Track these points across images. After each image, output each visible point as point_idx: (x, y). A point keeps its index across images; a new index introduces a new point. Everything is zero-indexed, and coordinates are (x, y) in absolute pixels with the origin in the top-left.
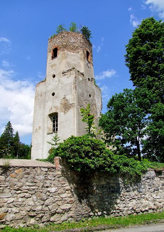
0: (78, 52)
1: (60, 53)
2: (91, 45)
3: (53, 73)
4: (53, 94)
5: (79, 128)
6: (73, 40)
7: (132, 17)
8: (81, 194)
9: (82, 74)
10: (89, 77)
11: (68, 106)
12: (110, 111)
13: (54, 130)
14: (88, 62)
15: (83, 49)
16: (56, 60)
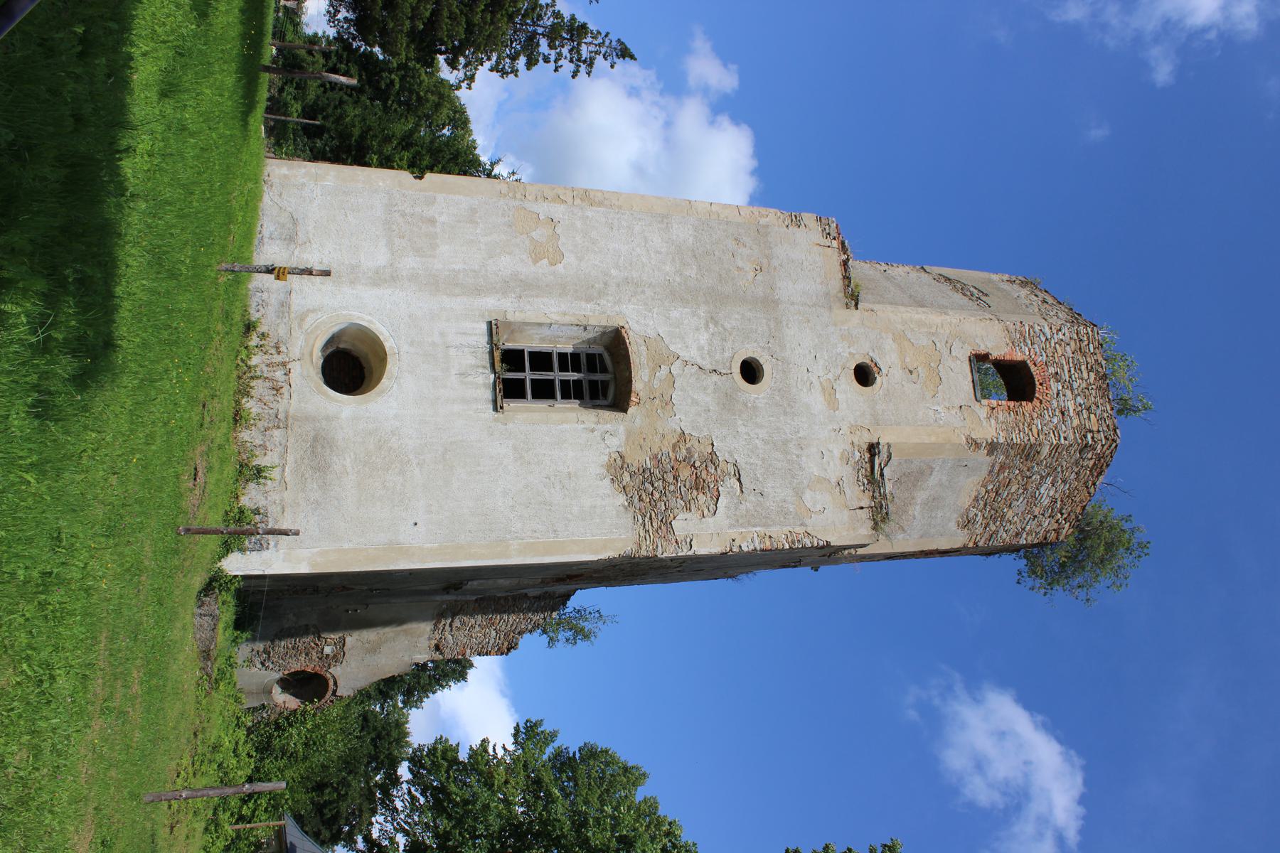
0: (968, 523)
3: (884, 371)
13: (512, 359)
16: (961, 378)
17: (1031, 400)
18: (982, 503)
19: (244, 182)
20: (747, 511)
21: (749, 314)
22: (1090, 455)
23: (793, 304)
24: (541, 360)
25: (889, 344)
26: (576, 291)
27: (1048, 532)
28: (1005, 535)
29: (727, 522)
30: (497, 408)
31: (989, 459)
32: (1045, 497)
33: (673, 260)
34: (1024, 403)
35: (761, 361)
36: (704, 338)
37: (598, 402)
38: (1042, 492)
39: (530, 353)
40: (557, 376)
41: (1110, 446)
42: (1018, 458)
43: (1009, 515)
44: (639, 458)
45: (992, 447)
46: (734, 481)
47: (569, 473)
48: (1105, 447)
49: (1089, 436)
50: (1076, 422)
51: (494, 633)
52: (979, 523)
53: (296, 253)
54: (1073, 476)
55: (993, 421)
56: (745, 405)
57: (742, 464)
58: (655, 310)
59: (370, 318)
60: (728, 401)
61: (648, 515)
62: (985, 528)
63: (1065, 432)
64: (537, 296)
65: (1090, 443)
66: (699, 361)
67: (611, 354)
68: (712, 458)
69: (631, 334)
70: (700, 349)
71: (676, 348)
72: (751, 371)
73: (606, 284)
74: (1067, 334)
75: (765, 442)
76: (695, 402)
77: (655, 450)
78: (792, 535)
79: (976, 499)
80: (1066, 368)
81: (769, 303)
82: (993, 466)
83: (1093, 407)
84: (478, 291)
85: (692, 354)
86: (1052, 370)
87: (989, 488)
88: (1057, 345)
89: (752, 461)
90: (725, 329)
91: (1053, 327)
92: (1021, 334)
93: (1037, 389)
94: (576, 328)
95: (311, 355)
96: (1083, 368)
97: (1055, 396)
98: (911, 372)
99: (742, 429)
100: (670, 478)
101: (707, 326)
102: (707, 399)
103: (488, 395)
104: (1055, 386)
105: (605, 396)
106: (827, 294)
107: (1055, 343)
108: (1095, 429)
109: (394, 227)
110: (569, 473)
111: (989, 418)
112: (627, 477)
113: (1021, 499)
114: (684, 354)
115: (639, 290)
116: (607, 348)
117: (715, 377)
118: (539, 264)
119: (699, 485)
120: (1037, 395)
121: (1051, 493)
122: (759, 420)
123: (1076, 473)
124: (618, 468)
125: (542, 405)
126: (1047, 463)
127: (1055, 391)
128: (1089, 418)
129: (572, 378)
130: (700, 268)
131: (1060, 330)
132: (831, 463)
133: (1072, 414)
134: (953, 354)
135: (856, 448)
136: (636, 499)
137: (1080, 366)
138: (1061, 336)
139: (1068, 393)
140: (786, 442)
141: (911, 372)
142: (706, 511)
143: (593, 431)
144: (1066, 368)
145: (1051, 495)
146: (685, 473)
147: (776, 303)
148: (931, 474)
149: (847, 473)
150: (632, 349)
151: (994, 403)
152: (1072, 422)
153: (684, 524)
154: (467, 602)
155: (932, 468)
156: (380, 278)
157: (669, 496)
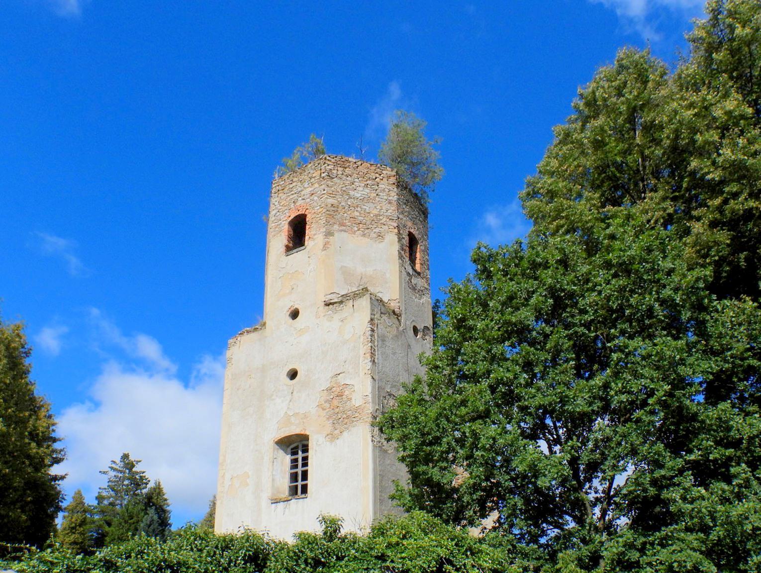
0: (380, 236)
1: (314, 235)
2: (425, 213)
3: (292, 304)
4: (293, 375)
5: (381, 486)
6: (361, 189)
7: (577, 485)
8: (710, 241)
9: (396, 315)
10: (414, 324)
11: (345, 416)
12: (63, 522)
13: (294, 491)
14: (415, 271)
15: (396, 225)
16: (299, 256)
17: (306, 215)
18: (367, 231)
22: (335, 172)
24: (294, 477)
27: (389, 184)
28: (390, 211)
31: (336, 234)
34: (307, 219)
38: (360, 195)
39: (291, 483)
42: (336, 217)
43: (375, 212)
44: (329, 428)
45: (329, 234)
46: (339, 377)
49: (323, 175)
50: (316, 185)
54: (349, 178)
55: (316, 236)
57: (332, 374)
61: (353, 419)
62: (384, 224)
65: (326, 174)
66: (288, 402)
67: (290, 444)
68: (329, 389)
69: (276, 436)
73: (256, 451)
74: (276, 200)
77: (325, 419)
79: (364, 235)
80: (291, 197)
83: (310, 176)
87: (356, 229)
92: (276, 228)
94: (275, 463)
96: (291, 186)
98: (293, 289)
100: (337, 410)
104: (300, 202)
108: (319, 172)
112: (337, 432)
113: (365, 207)
116: (288, 446)
117: (295, 393)
119: (340, 395)
120: (303, 213)
124: (332, 437)
126: (340, 198)
127: (302, 201)
133: (312, 189)
134: (284, 266)
135: (327, 313)
141: (293, 289)
142: (352, 390)
143: (316, 451)
144: (291, 197)
145: (362, 189)
146: (336, 402)
148: (346, 267)
149: (337, 317)
150: (287, 434)
153: (357, 400)
155: (342, 267)
157: (345, 409)
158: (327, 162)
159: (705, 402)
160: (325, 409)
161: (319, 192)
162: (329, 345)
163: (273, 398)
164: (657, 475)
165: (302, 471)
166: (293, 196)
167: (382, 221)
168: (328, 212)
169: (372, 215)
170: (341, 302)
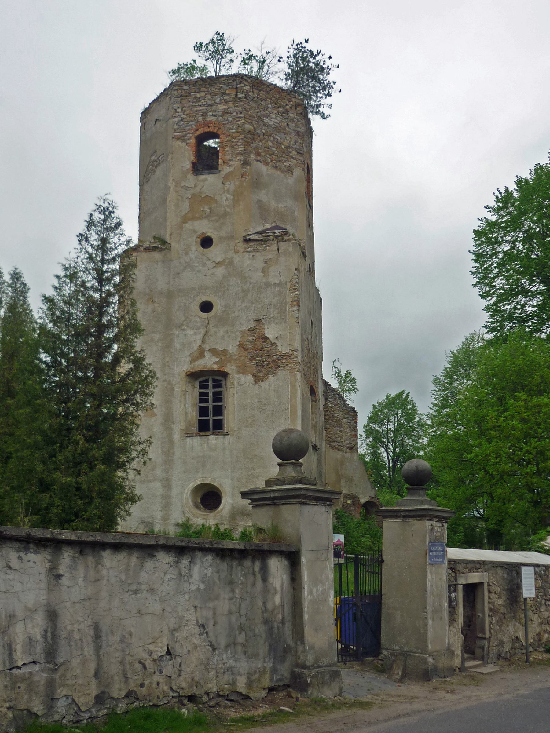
13: (203, 426)
19: (125, 497)
20: (278, 313)
21: (176, 307)
22: (251, 94)
23: (169, 282)
24: (203, 411)
25: (188, 226)
26: (169, 395)
29: (283, 325)
30: (227, 434)
32: (276, 121)
33: (150, 346)
35: (201, 301)
36: (190, 332)
37: (223, 385)
40: (211, 404)
41: (246, 80)
47: (258, 402)
48: (246, 83)
50: (231, 104)
51: (344, 420)
52: (290, 163)
53: (157, 521)
55: (231, 163)
56: (224, 312)
58: (177, 356)
59: (186, 490)
60: (222, 320)
63: (237, 113)
64: (172, 414)
66: (202, 335)
70: (195, 334)
71: (195, 347)
72: (206, 307)
75: (243, 301)
76: (223, 337)
78: (291, 290)
80: (199, 108)
81: (169, 295)
82: (257, 161)
84: (171, 442)
85: (198, 339)
86: (200, 118)
88: (185, 113)
89: (253, 309)
90: (185, 320)
91: (174, 115)
93: (212, 131)
95: (204, 515)
97: (215, 118)
99: (237, 314)
101: (183, 330)
102: (221, 331)
103: (221, 437)
105: (220, 381)
106: (163, 262)
107: (184, 114)
109: (143, 479)
110: (258, 402)
111: (229, 166)
114: (199, 342)
115: (167, 364)
116: (196, 379)
117: (210, 326)
118: (157, 413)
120: (215, 131)
121: (274, 116)
122: (232, 305)
123: (262, 101)
125: (225, 412)
127: (213, 118)
128: (228, 94)
129: (212, 397)
130: (153, 332)
131: (176, 110)
132: (254, 265)
136: (272, 370)
137: (197, 98)
138: (179, 110)
139: (214, 108)
140: (243, 290)
144: (199, 108)
147: (169, 291)
151: (220, 161)
152: (231, 107)
154: (327, 436)
156: (167, 484)
158: (244, 82)
159: (10, 282)
160: (247, 350)
161: (235, 114)
162: (250, 284)
163: (183, 328)
164: (10, 688)
165: (213, 406)
166: (201, 108)
167: (291, 154)
168: (246, 140)
169: (283, 147)
170: (262, 242)
